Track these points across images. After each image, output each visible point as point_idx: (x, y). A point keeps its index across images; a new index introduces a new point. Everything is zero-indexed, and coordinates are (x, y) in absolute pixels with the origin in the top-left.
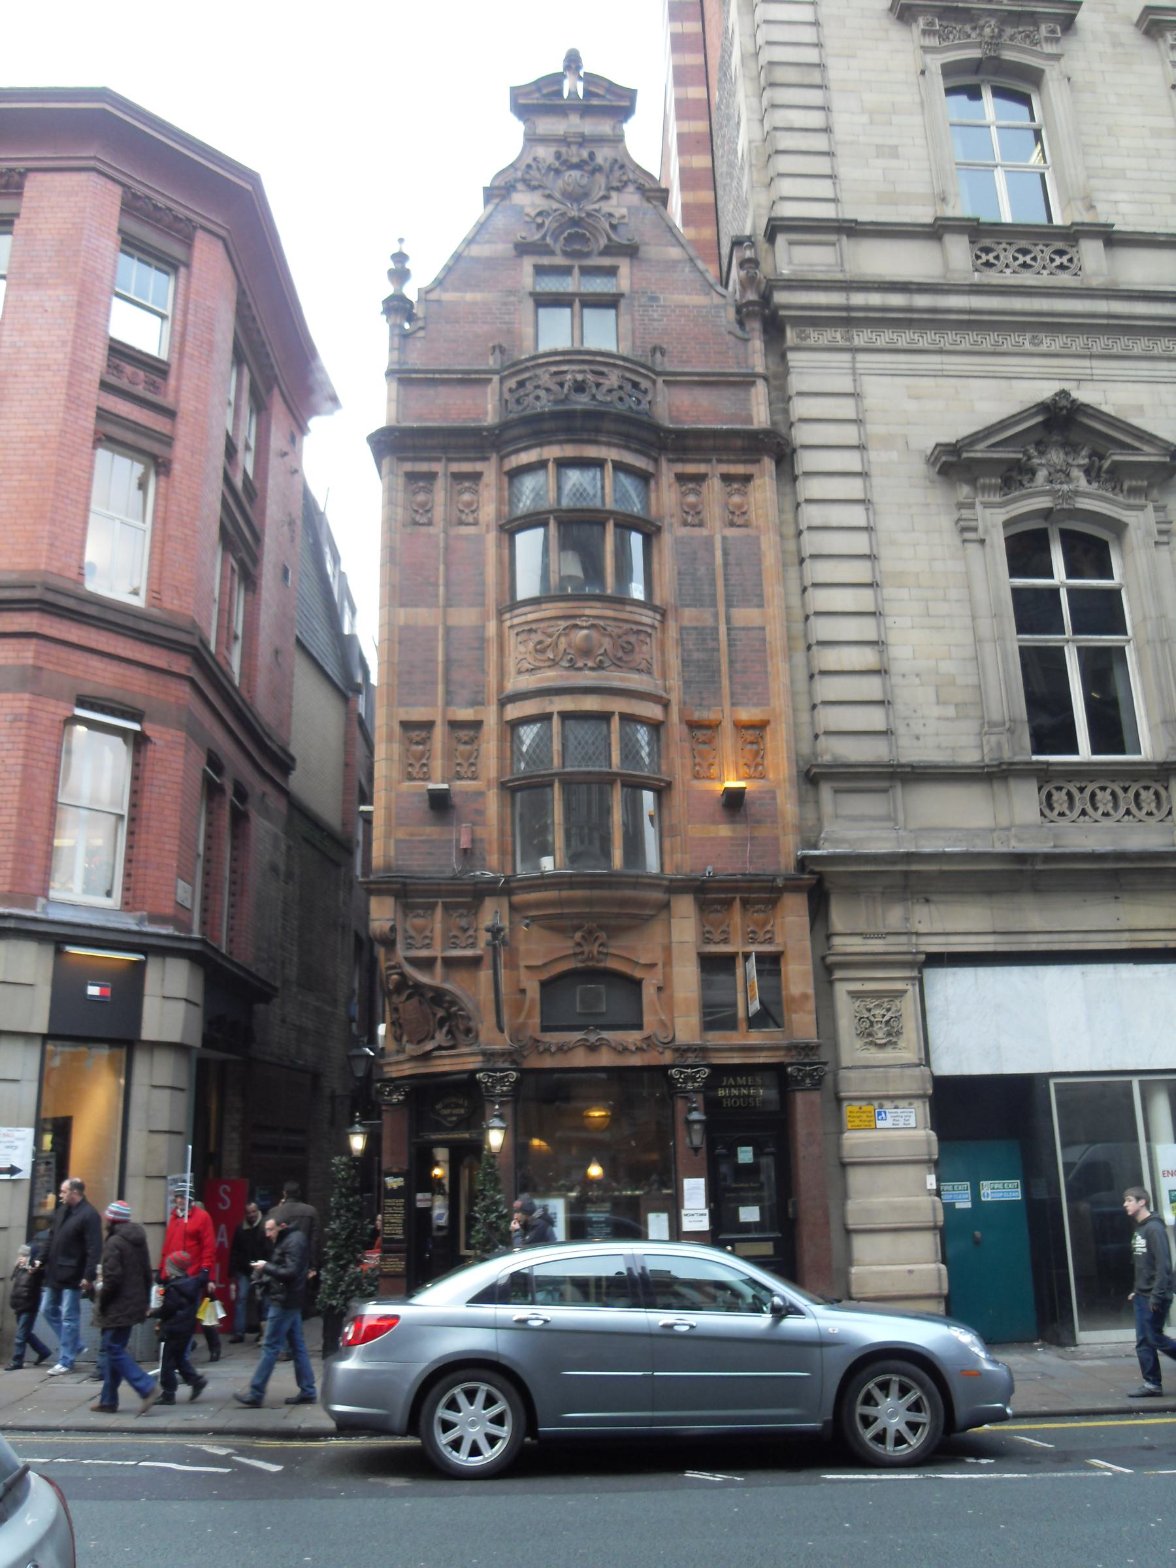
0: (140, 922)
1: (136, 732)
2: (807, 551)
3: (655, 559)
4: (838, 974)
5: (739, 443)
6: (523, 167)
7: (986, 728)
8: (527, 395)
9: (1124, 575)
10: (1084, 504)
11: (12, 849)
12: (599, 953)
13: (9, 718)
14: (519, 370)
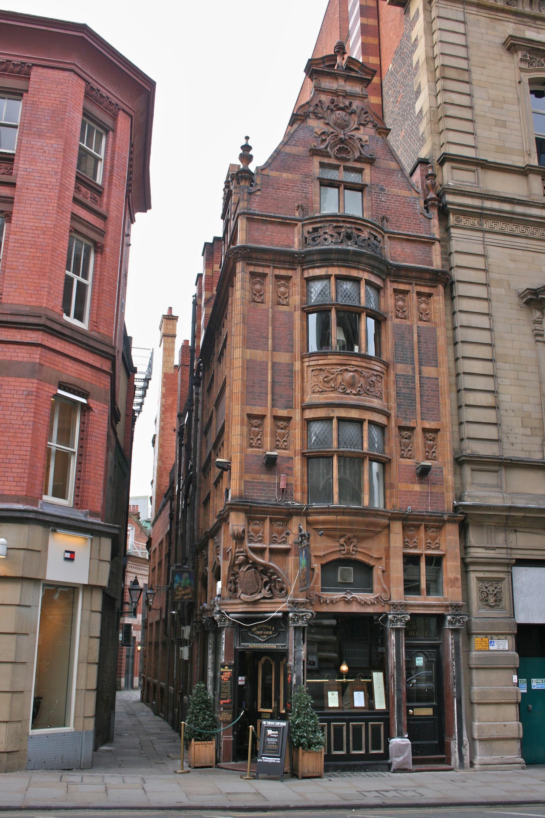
0: (86, 516)
1: (83, 404)
2: (459, 338)
4: (472, 568)
5: (428, 276)
6: (314, 105)
8: (319, 237)
11: (27, 471)
12: (353, 550)
13: (25, 393)
14: (319, 223)
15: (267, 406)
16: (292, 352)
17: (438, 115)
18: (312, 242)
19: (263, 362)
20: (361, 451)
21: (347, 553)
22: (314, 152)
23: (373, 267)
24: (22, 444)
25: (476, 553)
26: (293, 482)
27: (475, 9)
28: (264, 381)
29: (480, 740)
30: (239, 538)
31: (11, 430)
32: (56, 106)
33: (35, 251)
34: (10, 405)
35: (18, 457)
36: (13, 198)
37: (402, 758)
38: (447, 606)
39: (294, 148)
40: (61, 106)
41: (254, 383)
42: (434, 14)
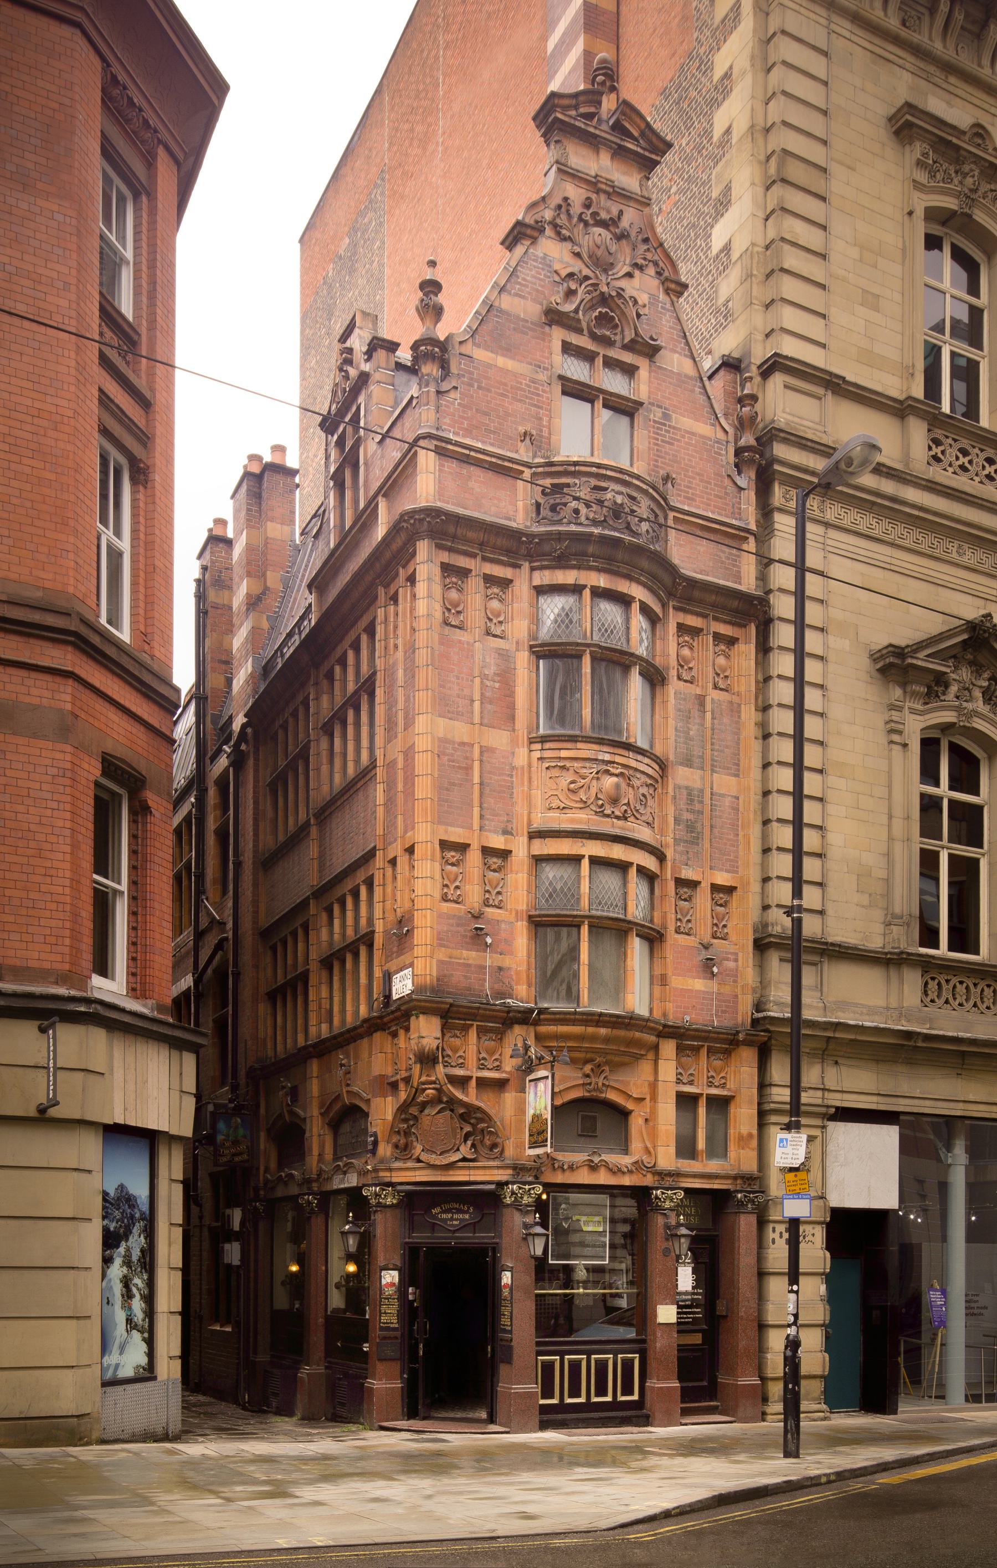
4: (774, 1119)
10: (979, 724)
22: (554, 317)
27: (847, 24)
30: (428, 1059)
31: (32, 844)
33: (41, 465)
34: (25, 792)
39: (517, 300)
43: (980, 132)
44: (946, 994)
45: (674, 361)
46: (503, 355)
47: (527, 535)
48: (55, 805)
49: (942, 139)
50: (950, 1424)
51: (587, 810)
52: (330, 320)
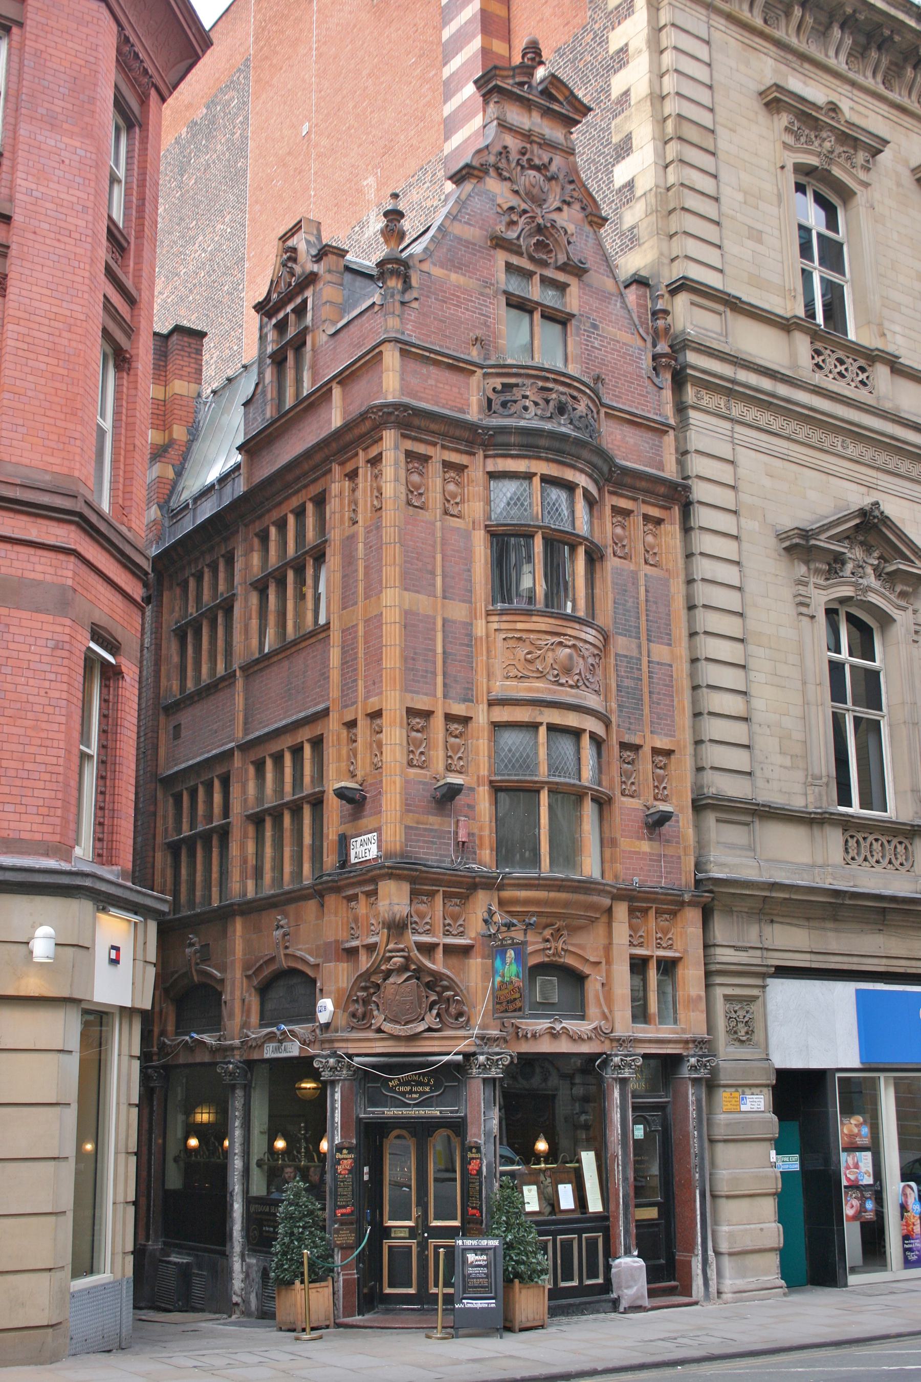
2: (700, 600)
3: (598, 583)
4: (719, 980)
5: (662, 490)
7: (809, 779)
8: (515, 402)
9: (884, 659)
10: (873, 598)
13: (51, 644)
15: (435, 696)
16: (470, 602)
17: (669, 205)
18: (501, 410)
19: (428, 616)
20: (577, 782)
21: (554, 955)
23: (594, 466)
24: (49, 743)
25: (724, 955)
26: (476, 831)
27: (723, 21)
28: (430, 650)
29: (731, 1254)
30: (397, 927)
31: (30, 715)
32: (78, 68)
33: (55, 362)
35: (42, 768)
36: (8, 247)
37: (635, 1289)
38: (686, 1042)
39: (466, 227)
40: (87, 72)
41: (415, 653)
42: (665, 17)
43: (834, 108)
44: (864, 852)
45: (598, 278)
46: (456, 272)
47: (482, 428)
48: (53, 676)
49: (803, 112)
50: (868, 1301)
51: (543, 679)
52: (182, 176)
